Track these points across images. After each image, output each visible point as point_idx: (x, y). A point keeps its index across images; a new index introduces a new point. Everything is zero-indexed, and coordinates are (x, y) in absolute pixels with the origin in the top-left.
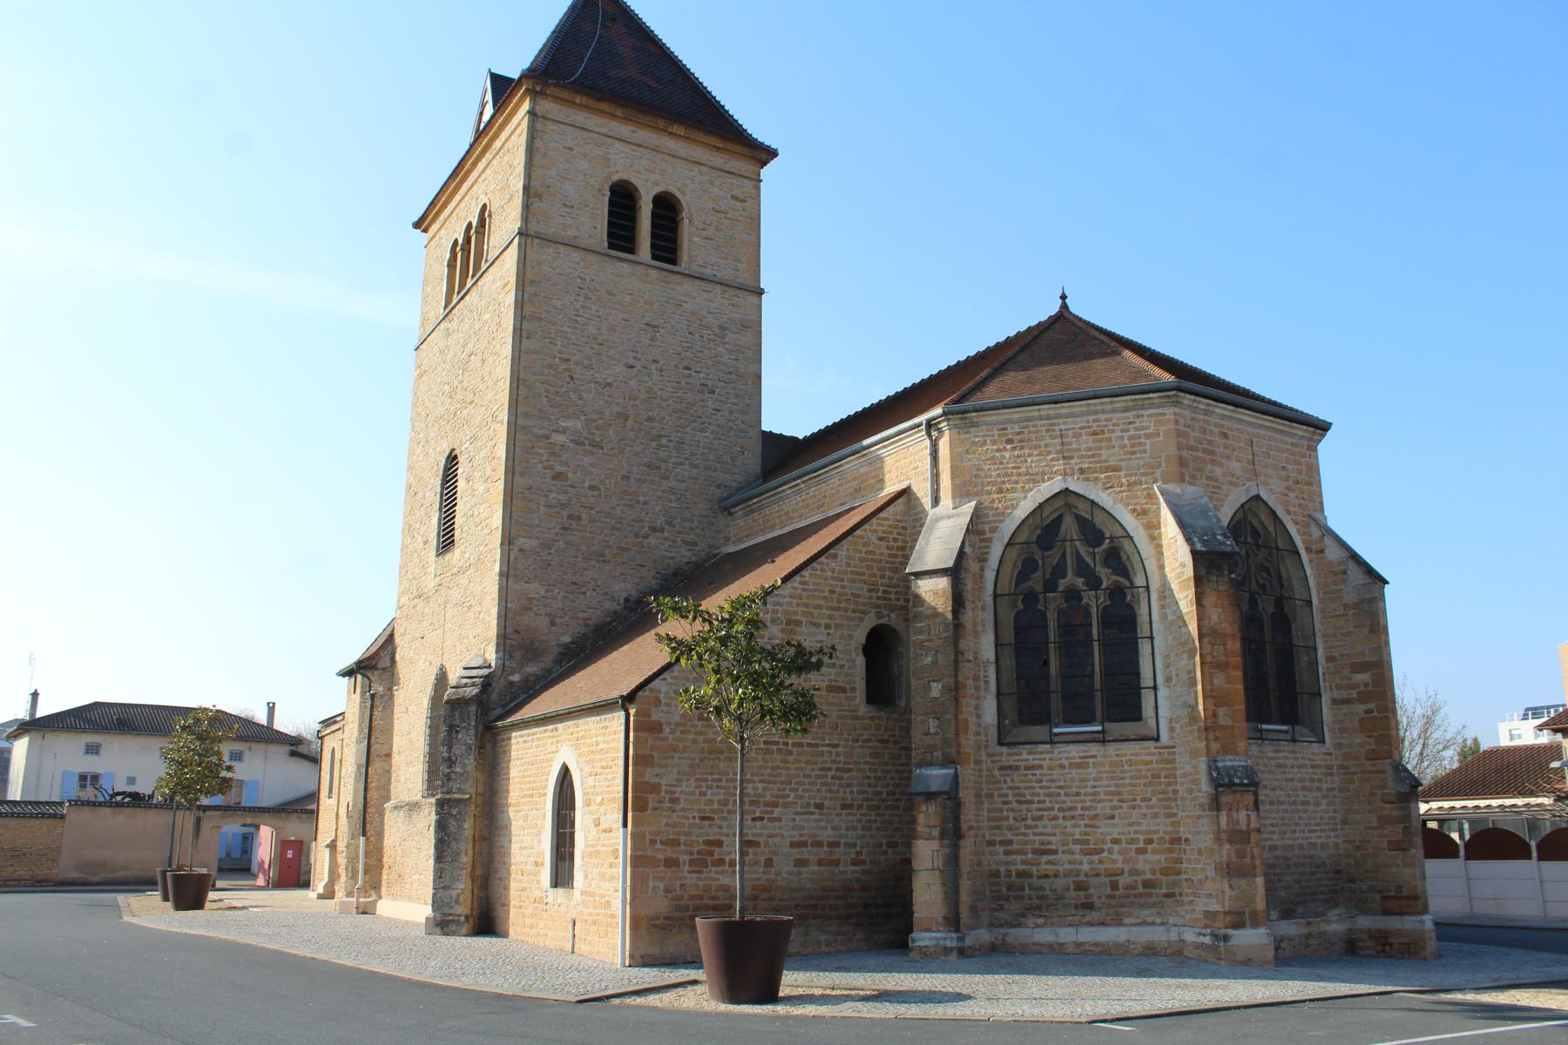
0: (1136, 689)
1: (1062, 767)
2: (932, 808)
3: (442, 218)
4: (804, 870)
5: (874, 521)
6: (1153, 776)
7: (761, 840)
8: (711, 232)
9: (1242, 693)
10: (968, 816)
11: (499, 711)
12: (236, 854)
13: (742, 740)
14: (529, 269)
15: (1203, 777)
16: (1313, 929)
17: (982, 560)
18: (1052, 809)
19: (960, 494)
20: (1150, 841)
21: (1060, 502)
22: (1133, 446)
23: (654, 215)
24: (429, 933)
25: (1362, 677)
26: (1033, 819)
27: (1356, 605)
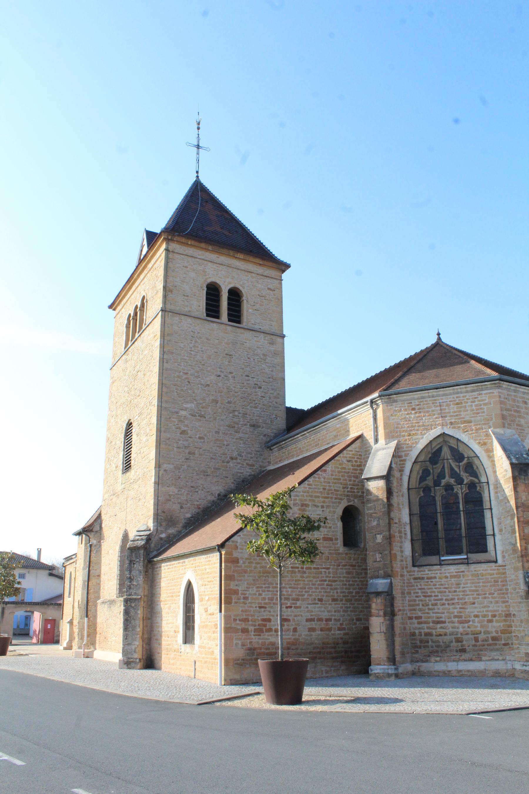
0: (483, 536)
1: (446, 577)
3: (123, 303)
4: (313, 633)
5: (345, 452)
6: (495, 581)
8: (258, 306)
10: (398, 604)
11: (155, 553)
12: (22, 626)
13: (280, 567)
14: (167, 329)
17: (401, 471)
18: (442, 599)
19: (389, 437)
20: (494, 616)
21: (441, 440)
23: (229, 299)
26: (432, 605)
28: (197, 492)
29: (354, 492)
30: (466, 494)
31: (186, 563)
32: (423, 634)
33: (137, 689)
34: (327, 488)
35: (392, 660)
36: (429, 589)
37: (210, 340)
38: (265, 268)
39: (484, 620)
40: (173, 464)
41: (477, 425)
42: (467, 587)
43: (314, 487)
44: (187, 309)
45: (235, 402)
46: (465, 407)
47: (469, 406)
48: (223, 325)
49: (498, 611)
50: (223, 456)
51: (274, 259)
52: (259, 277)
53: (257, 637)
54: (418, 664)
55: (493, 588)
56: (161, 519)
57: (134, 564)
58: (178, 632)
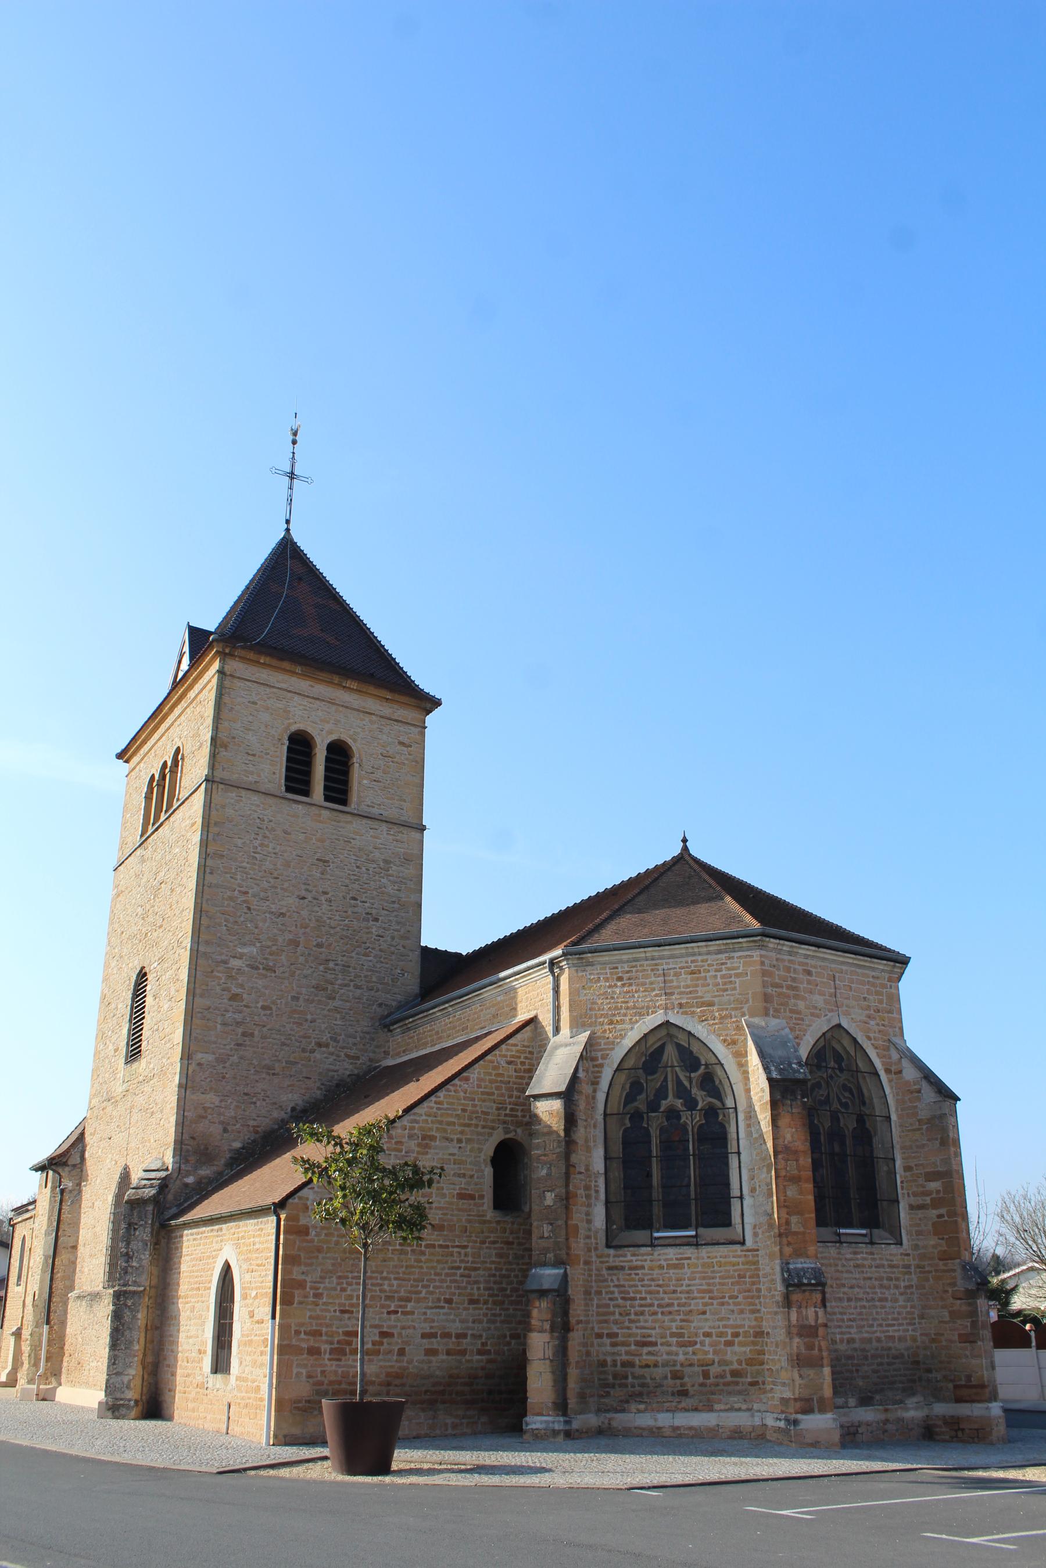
0: (725, 1199)
1: (661, 1267)
2: (544, 1304)
3: (142, 752)
4: (433, 1358)
5: (503, 1046)
6: (739, 1276)
7: (395, 1331)
8: (379, 774)
9: (813, 1204)
10: (577, 1310)
11: (174, 1210)
13: (365, 1245)
14: (214, 813)
15: (778, 1277)
16: (890, 1416)
17: (595, 1083)
18: (652, 1305)
19: (577, 1025)
20: (736, 1335)
21: (663, 1032)
22: (725, 984)
23: (328, 759)
24: (100, 1417)
25: (934, 1185)
26: (636, 1314)
27: (929, 1121)
28: (255, 1103)
29: (517, 1116)
30: (701, 1126)
31: (224, 1231)
32: (619, 1364)
33: (122, 1450)
34: (470, 1108)
35: (561, 1406)
36: (632, 1286)
37: (290, 834)
38: (396, 706)
39: (720, 1342)
40: (214, 1054)
41: (722, 1010)
42: (694, 1285)
43: (445, 1106)
44: (251, 778)
45: (330, 945)
46: (705, 978)
47: (711, 977)
48: (314, 808)
49: (743, 1326)
50: (304, 1041)
51: (414, 689)
52: (383, 721)
53: (335, 1363)
54: (608, 1415)
55: (736, 1288)
56: (188, 1151)
57: (135, 1229)
58: (205, 1352)
